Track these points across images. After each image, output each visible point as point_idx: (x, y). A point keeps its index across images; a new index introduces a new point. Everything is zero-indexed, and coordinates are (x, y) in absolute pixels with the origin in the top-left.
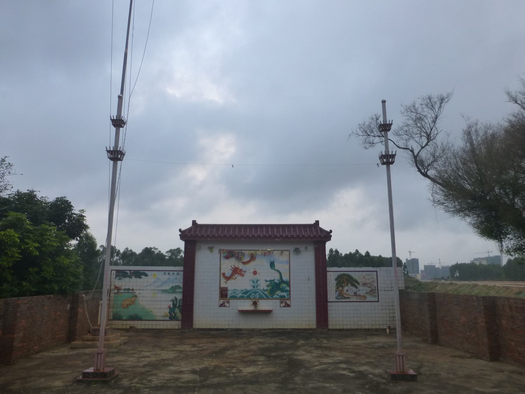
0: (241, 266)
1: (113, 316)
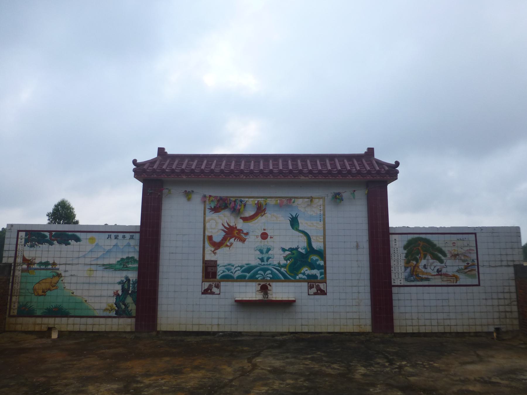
0: (240, 225)
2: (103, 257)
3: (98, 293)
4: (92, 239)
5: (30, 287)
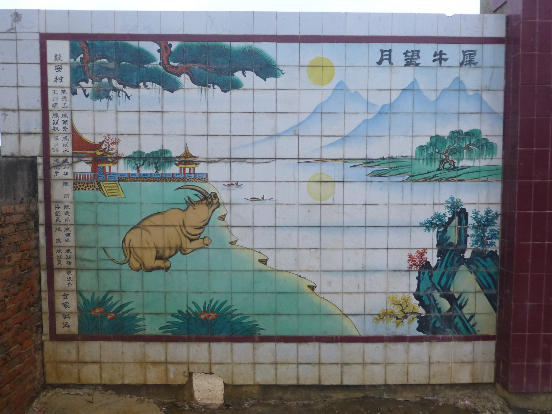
1: (84, 311)
2: (364, 133)
3: (354, 261)
5: (111, 239)
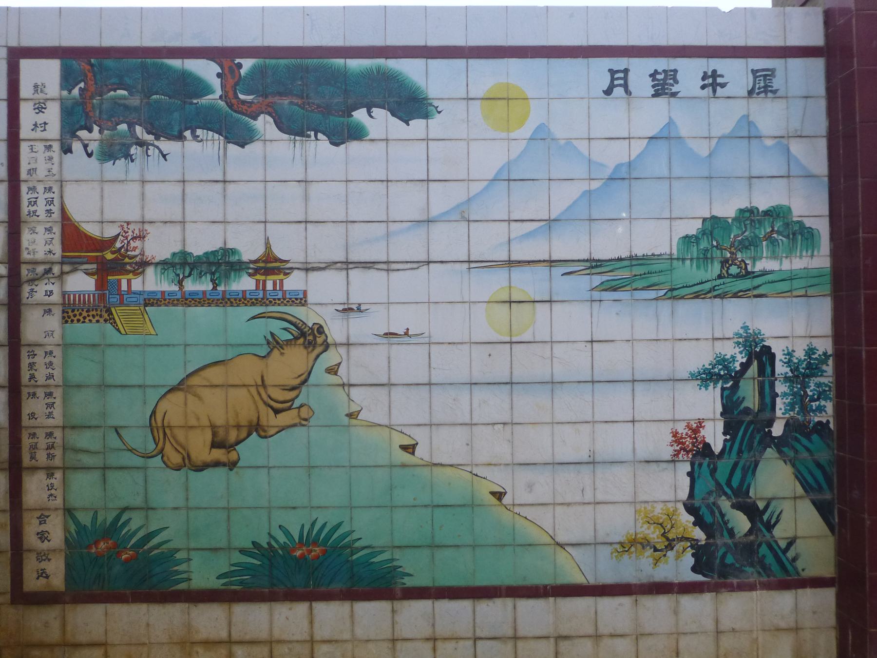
2: (586, 214)
3: (573, 444)
4: (503, 99)
5: (130, 412)
